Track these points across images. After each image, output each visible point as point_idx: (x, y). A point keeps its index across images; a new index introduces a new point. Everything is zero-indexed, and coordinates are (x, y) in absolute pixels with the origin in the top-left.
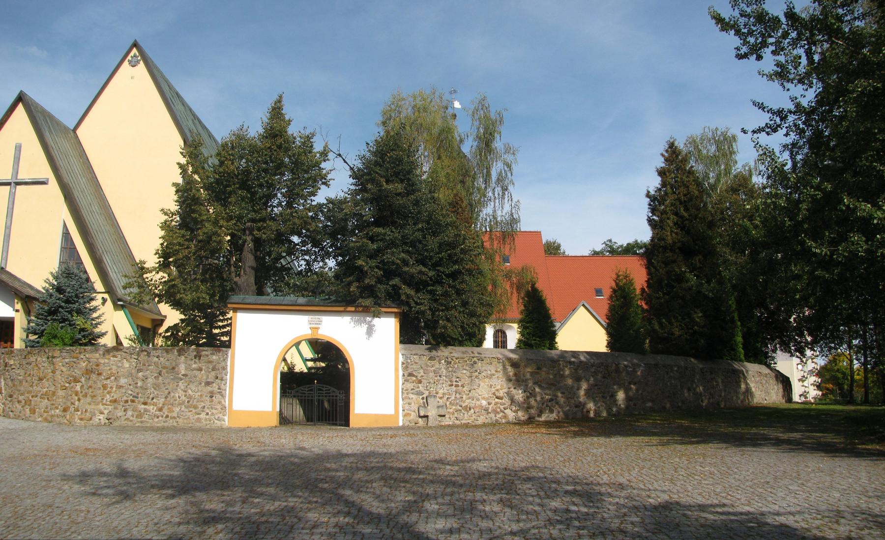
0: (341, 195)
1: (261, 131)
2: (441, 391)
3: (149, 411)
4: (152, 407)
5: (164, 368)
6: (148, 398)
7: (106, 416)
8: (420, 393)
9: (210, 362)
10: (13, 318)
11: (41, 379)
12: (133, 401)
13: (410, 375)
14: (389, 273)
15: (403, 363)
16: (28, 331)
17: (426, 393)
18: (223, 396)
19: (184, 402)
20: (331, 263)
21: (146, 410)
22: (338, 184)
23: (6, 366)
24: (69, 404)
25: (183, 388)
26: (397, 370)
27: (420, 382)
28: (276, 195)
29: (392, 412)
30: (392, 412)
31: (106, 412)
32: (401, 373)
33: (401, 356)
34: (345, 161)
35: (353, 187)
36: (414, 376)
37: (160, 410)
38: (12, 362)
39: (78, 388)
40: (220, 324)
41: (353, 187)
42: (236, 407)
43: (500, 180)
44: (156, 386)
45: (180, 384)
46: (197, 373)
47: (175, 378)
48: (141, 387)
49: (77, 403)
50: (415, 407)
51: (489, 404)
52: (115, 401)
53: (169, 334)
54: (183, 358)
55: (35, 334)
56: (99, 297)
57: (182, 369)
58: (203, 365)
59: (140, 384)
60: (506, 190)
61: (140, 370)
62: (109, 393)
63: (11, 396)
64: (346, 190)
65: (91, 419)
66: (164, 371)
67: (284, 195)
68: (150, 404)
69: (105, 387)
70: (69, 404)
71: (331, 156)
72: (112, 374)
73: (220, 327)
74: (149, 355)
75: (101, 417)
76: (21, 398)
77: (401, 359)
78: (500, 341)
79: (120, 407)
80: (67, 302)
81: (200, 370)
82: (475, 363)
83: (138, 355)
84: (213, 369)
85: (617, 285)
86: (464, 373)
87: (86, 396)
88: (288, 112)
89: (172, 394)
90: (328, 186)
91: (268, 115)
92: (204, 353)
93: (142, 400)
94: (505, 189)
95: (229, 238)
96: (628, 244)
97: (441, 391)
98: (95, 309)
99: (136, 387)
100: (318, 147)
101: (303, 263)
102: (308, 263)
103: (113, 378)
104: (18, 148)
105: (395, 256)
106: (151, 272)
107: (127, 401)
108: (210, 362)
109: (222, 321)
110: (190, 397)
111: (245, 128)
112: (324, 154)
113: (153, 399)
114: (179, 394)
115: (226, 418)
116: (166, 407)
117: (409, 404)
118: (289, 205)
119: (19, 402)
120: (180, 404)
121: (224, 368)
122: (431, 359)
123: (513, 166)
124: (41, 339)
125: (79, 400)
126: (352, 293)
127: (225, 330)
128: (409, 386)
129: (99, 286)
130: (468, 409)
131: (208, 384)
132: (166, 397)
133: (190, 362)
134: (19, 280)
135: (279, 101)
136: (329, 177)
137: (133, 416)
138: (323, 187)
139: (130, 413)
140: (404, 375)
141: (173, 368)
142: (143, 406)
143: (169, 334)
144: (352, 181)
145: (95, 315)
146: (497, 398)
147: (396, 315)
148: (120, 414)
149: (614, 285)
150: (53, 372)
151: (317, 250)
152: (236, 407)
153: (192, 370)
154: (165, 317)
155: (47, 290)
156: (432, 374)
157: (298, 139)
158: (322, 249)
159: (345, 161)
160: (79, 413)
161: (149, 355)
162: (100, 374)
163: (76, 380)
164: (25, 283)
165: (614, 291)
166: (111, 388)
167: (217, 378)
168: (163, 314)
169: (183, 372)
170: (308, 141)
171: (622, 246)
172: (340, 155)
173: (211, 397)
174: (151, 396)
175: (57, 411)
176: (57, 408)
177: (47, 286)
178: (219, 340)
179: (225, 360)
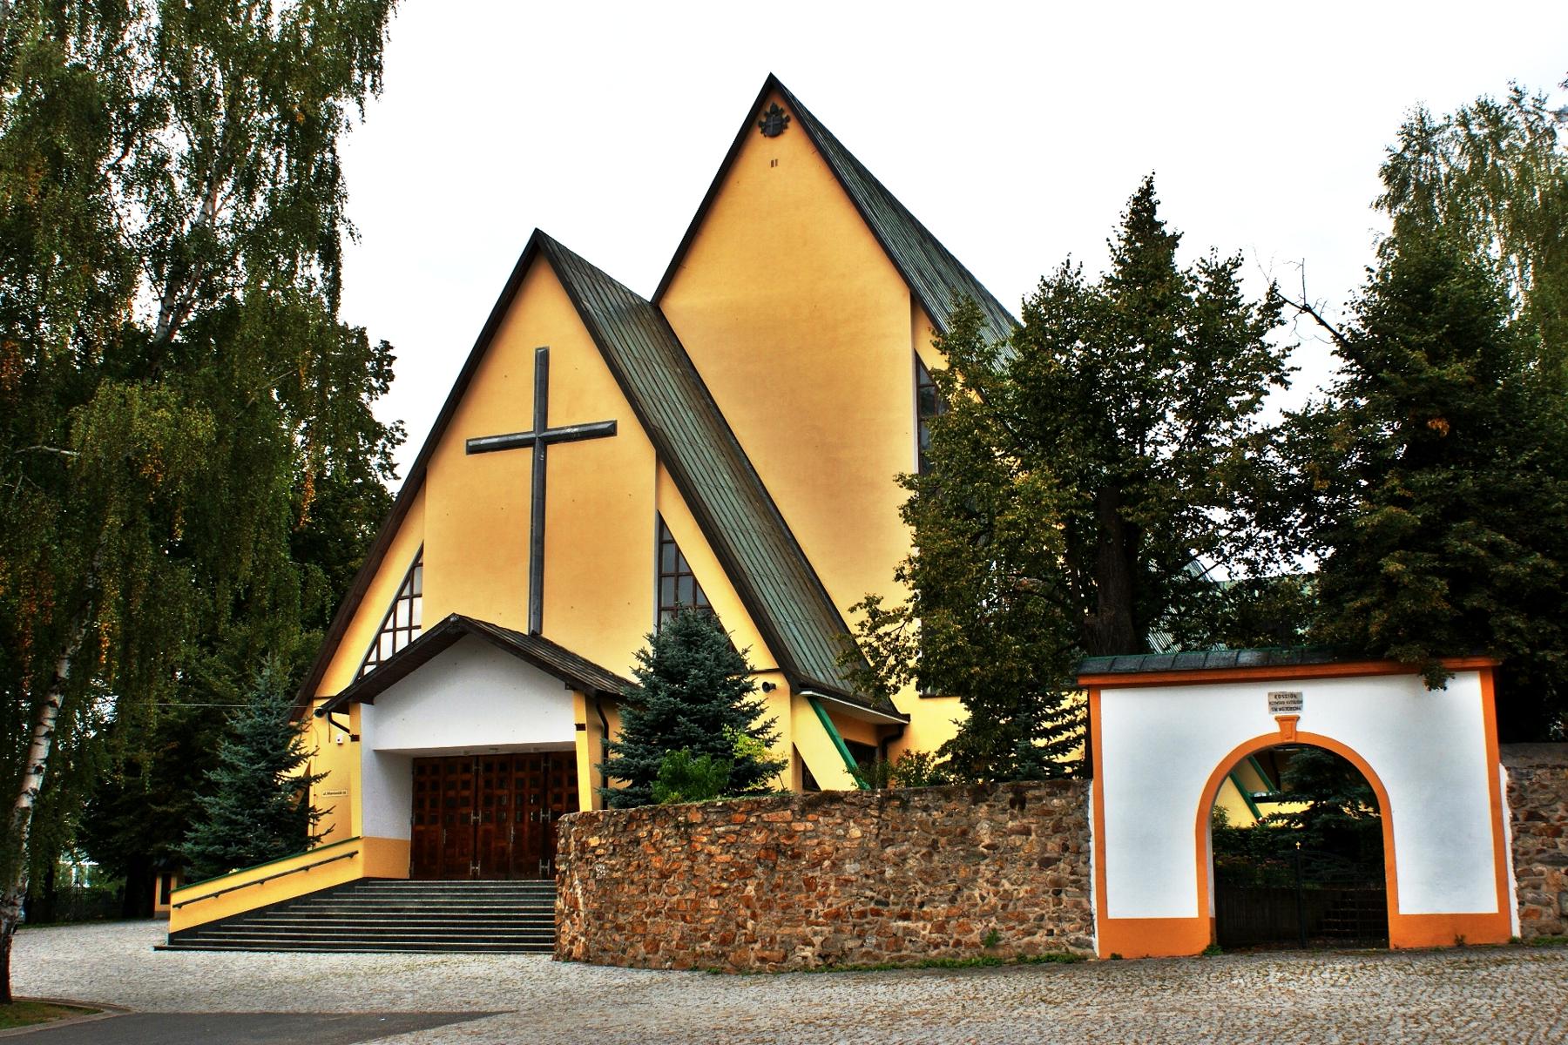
0: (1319, 401)
1: (1111, 269)
3: (917, 934)
4: (921, 924)
5: (943, 833)
6: (911, 903)
10: (573, 744)
11: (664, 876)
12: (877, 913)
13: (1532, 816)
14: (1465, 576)
15: (1510, 790)
16: (606, 770)
18: (1085, 891)
19: (994, 908)
20: (1309, 563)
22: (1313, 376)
23: (583, 851)
24: (732, 926)
25: (989, 875)
28: (1162, 417)
31: (818, 940)
32: (1507, 814)
34: (1322, 323)
35: (1346, 378)
36: (1542, 818)
37: (940, 928)
38: (594, 841)
39: (750, 890)
40: (1047, 725)
41: (1346, 378)
42: (1114, 912)
44: (928, 876)
45: (982, 868)
46: (1017, 840)
48: (893, 880)
52: (837, 915)
53: (948, 757)
54: (984, 809)
55: (626, 777)
56: (759, 681)
58: (1030, 821)
61: (890, 842)
62: (822, 898)
64: (1330, 386)
65: (785, 957)
66: (943, 840)
67: (1180, 414)
68: (919, 918)
69: (810, 885)
71: (1286, 312)
72: (825, 856)
73: (1045, 733)
75: (808, 952)
76: (621, 920)
77: (1504, 777)
78: (1128, 515)
80: (692, 698)
81: (1026, 832)
83: (881, 808)
84: (1057, 829)
87: (768, 906)
88: (1169, 216)
89: (966, 892)
90: (1286, 384)
91: (1122, 231)
93: (897, 909)
95: (1061, 527)
98: (754, 712)
99: (883, 881)
100: (1252, 292)
101: (1243, 568)
102: (1252, 565)
103: (827, 863)
104: (543, 358)
106: (894, 620)
107: (863, 914)
108: (1049, 813)
109: (1050, 718)
110: (1007, 897)
111: (1074, 268)
112: (1273, 306)
113: (922, 905)
114: (980, 889)
115: (1095, 940)
116: (953, 922)
117: (1536, 887)
118: (1197, 434)
119: (619, 928)
120: (984, 915)
121: (1082, 825)
124: (639, 786)
125: (754, 916)
126: (1360, 629)
127: (1060, 738)
128: (1530, 843)
129: (758, 656)
131: (1046, 863)
132: (953, 900)
133: (1000, 817)
134: (573, 657)
135: (1147, 192)
136: (1287, 363)
138: (1276, 389)
139: (872, 941)
140: (1514, 818)
141: (964, 833)
142: (901, 923)
143: (948, 757)
144: (1340, 363)
145: (755, 725)
147: (1483, 671)
148: (850, 944)
150: (692, 856)
151: (1271, 534)
152: (1114, 912)
154: (907, 717)
155: (644, 678)
157: (1203, 277)
158: (1283, 532)
159: (1322, 323)
160: (757, 946)
162: (797, 857)
163: (745, 873)
164: (587, 664)
166: (826, 885)
168: (901, 711)
169: (987, 841)
170: (1222, 278)
172: (1306, 309)
173: (1057, 893)
174: (918, 899)
175: (708, 944)
176: (706, 938)
177: (643, 666)
178: (1050, 763)
179: (1083, 806)
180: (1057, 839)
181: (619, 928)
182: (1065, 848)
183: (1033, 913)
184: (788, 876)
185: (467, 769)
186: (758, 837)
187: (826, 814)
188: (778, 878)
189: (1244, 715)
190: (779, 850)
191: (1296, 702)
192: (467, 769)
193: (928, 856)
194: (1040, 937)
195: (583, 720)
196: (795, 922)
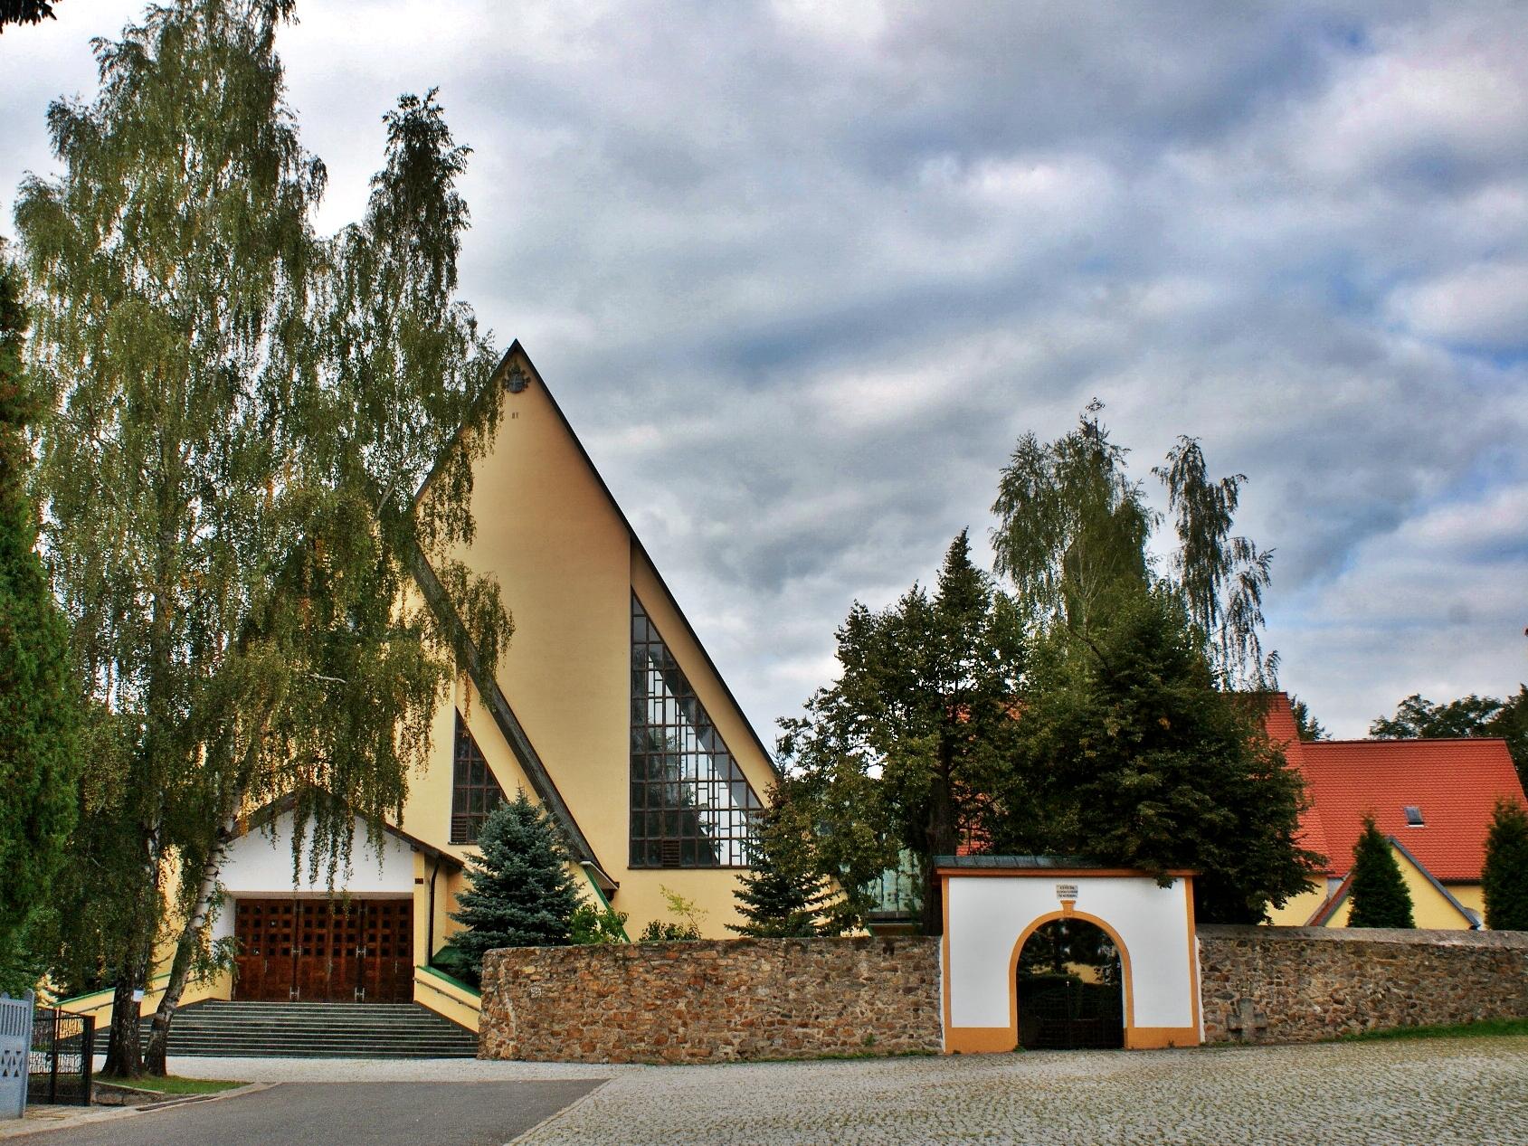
2: (1257, 993)
7: (737, 1047)
8: (1227, 996)
9: (910, 958)
12: (784, 1023)
13: (1213, 968)
17: (1237, 996)
18: (936, 1008)
21: (806, 1035)
24: (665, 1032)
26: (1192, 962)
27: (1227, 979)
29: (1190, 1024)
30: (1190, 1024)
31: (736, 1041)
33: (1197, 942)
37: (831, 1033)
38: (529, 970)
39: (682, 1006)
43: (1239, 610)
46: (889, 975)
47: (853, 985)
49: (681, 1030)
50: (1220, 1015)
51: (1326, 1011)
52: (752, 1024)
54: (864, 953)
57: (864, 969)
59: (792, 995)
60: (1247, 631)
62: (740, 1012)
63: (533, 1025)
68: (814, 1026)
69: (730, 1002)
70: (665, 1032)
74: (804, 950)
75: (729, 1049)
76: (556, 1028)
79: (760, 1033)
81: (895, 970)
82: (1303, 949)
84: (917, 968)
85: (1498, 822)
86: (1288, 965)
87: (697, 1017)
92: (897, 944)
94: (1244, 630)
96: (1456, 704)
97: (1257, 993)
105: (1188, 796)
107: (772, 1024)
108: (910, 958)
115: (943, 1042)
117: (1214, 1012)
119: (554, 1034)
120: (863, 1024)
121: (935, 966)
122: (1242, 944)
123: (1262, 588)
125: (685, 1024)
128: (1212, 985)
130: (1295, 1018)
131: (908, 991)
132: (840, 1014)
135: (963, 541)
137: (784, 1045)
139: (778, 1042)
141: (849, 969)
146: (1337, 1002)
148: (761, 1044)
149: (1492, 821)
153: (880, 971)
156: (1242, 968)
161: (804, 950)
163: (676, 993)
165: (1493, 832)
166: (743, 1003)
167: (923, 981)
171: (1442, 708)
173: (916, 1010)
176: (642, 1040)
179: (935, 953)
180: (917, 974)
181: (554, 1034)
182: (923, 981)
183: (899, 1023)
184: (712, 996)
185: (288, 910)
186: (689, 969)
187: (744, 954)
188: (705, 997)
189: (1035, 900)
190: (705, 978)
191: (1074, 891)
192: (288, 910)
193: (821, 984)
194: (904, 1039)
195: (422, 876)
196: (719, 1029)
